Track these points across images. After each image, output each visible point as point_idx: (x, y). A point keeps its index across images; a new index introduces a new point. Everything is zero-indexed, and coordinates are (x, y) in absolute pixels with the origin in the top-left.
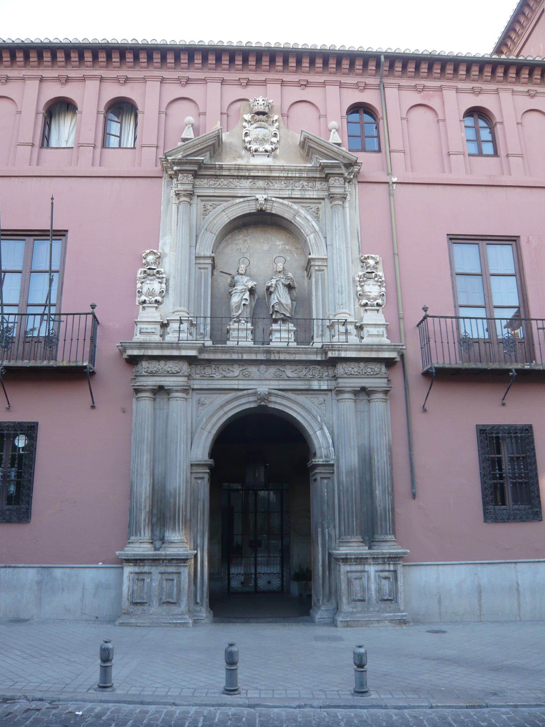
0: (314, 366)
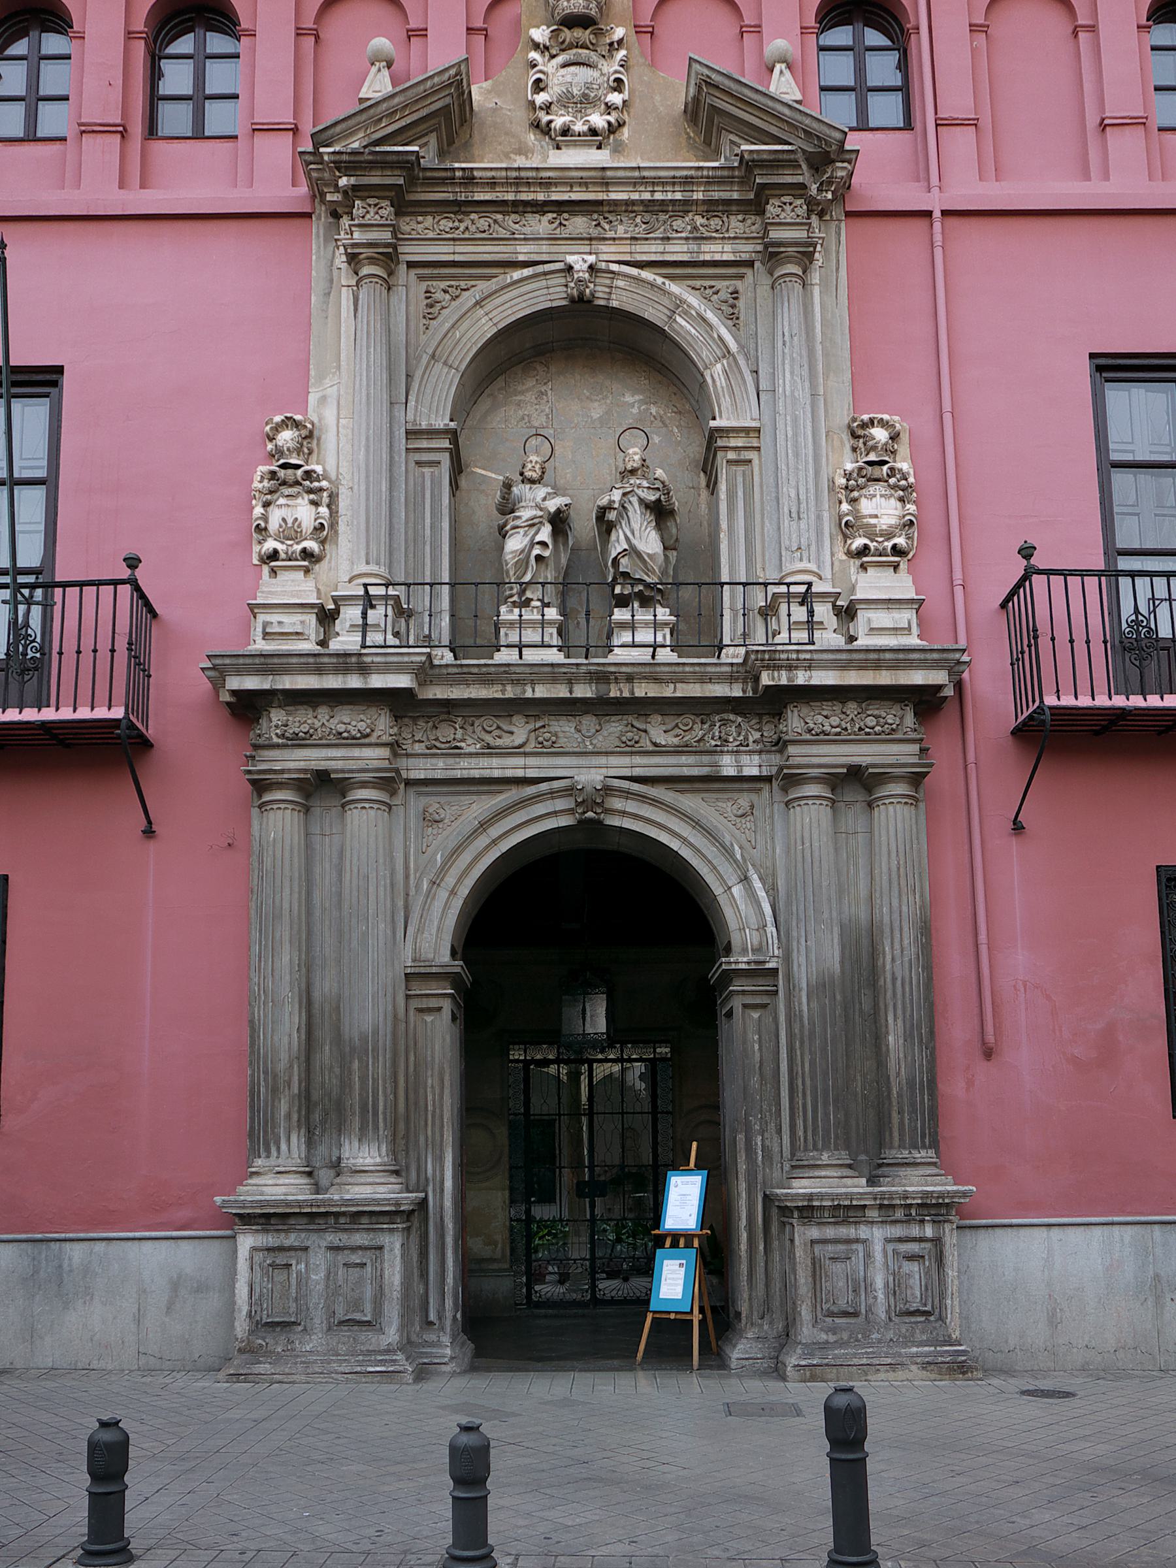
0: (725, 716)
